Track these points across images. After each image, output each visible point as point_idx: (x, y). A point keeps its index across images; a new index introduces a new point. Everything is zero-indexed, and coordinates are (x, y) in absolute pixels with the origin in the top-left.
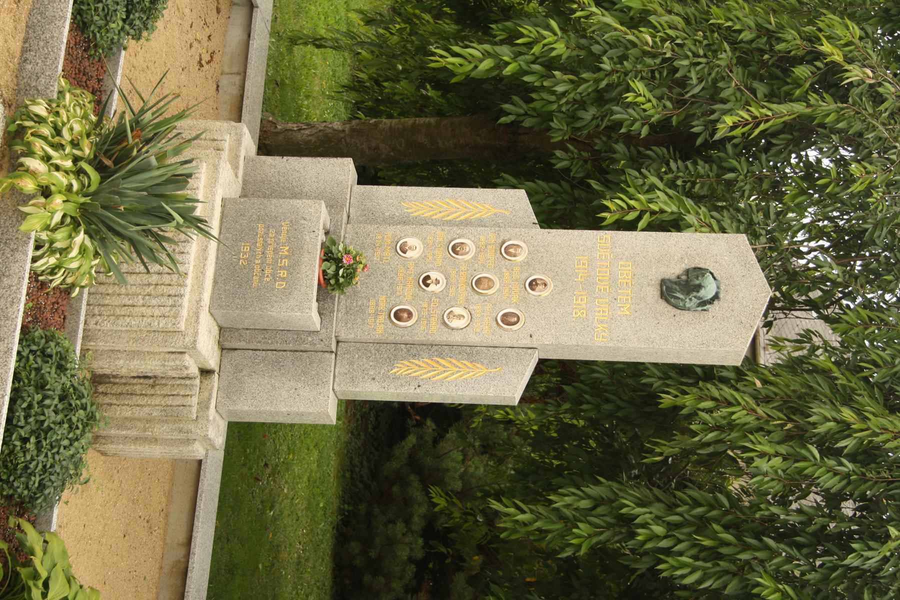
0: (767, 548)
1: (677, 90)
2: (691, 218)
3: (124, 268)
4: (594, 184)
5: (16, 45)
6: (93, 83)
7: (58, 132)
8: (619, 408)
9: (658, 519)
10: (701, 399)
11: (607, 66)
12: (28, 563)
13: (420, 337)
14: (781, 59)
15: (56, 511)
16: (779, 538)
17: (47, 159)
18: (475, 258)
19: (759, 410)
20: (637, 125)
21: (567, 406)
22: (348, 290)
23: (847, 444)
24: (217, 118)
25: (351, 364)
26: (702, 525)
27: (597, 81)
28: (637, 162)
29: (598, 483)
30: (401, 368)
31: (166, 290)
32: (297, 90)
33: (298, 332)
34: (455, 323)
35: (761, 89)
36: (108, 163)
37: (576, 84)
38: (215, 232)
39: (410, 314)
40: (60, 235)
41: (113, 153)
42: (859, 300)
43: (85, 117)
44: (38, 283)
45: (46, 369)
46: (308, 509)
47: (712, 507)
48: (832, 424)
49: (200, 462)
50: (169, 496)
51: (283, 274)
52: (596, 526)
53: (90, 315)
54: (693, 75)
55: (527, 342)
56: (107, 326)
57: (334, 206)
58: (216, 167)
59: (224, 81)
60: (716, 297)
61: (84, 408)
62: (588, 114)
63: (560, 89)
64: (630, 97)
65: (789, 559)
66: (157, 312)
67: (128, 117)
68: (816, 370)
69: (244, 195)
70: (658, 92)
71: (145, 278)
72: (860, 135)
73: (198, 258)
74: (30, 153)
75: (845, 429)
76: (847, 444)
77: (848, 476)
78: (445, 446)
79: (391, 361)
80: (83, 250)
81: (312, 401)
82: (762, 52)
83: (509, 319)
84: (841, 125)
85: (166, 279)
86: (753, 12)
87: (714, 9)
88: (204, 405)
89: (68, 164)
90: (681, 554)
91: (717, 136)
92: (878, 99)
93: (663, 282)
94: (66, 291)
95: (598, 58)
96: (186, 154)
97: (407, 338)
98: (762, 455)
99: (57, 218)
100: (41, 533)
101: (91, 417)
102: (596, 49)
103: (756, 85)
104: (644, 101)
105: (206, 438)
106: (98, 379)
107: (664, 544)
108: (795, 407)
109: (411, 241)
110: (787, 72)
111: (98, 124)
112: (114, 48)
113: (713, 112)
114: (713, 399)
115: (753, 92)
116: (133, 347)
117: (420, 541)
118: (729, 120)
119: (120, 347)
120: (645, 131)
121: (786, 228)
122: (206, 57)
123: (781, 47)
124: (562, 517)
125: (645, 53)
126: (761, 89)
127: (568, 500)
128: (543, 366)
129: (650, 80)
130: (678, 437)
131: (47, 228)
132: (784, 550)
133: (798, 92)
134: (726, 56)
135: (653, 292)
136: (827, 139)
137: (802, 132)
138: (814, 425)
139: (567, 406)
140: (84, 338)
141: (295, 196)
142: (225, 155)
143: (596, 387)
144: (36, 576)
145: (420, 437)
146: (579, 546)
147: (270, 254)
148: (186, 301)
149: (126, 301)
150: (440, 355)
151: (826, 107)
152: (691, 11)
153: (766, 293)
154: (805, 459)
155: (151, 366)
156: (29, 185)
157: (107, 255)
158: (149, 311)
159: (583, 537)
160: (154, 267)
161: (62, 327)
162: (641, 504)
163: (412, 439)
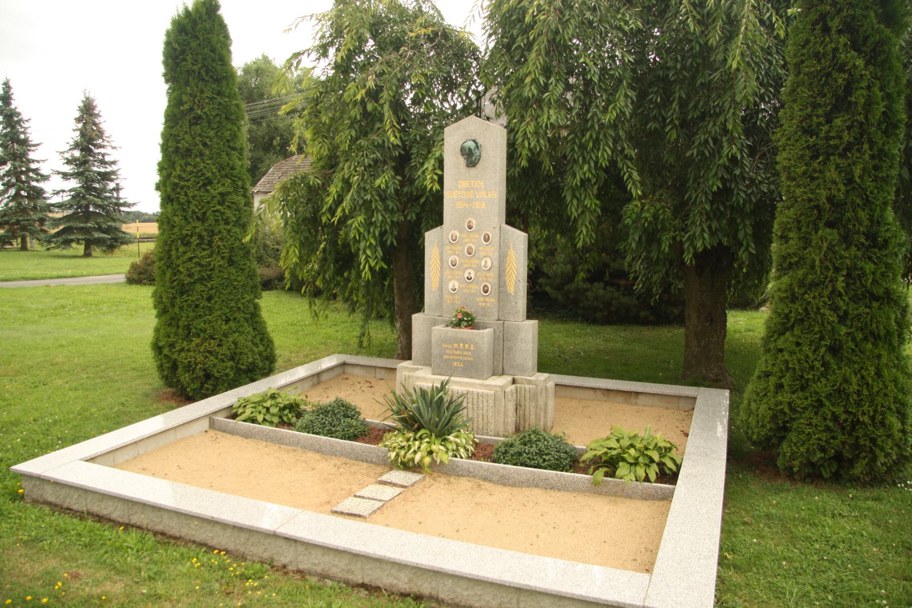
0: (592, 117)
1: (379, 164)
2: (437, 154)
3: (465, 419)
4: (422, 200)
5: (365, 465)
6: (380, 433)
7: (403, 447)
8: (530, 187)
9: (581, 168)
10: (524, 147)
11: (368, 197)
12: (600, 457)
13: (496, 280)
14: (364, 117)
15: (577, 447)
16: (587, 111)
17: (415, 452)
18: (458, 255)
19: (528, 120)
20: (396, 182)
21: (531, 212)
22: (474, 315)
23: (542, 80)
24: (395, 379)
25: (509, 313)
26: (583, 147)
27: (376, 201)
28: (412, 181)
29: (565, 197)
30: (511, 290)
31: (475, 400)
32: (383, 345)
33: (495, 339)
34: (489, 264)
35: (378, 125)
36: (416, 426)
37: (378, 211)
38: (447, 378)
39: (485, 286)
40: (450, 447)
41: (412, 423)
42: (475, 78)
43: (396, 436)
44: (473, 456)
45: (512, 452)
46: (580, 337)
47: (575, 142)
48: (533, 87)
49: (556, 385)
50: (572, 398)
51: (467, 346)
52: (586, 196)
53: (487, 434)
54: (372, 156)
55: (497, 230)
56: (492, 427)
57: (434, 323)
58: (418, 378)
59: (379, 376)
60: (474, 141)
61: (530, 435)
62: (391, 205)
63: (380, 218)
64: (383, 186)
65: (597, 107)
66: (486, 404)
67: (395, 417)
68: (508, 96)
69: (430, 365)
70: (381, 173)
71: (470, 409)
72: (398, 80)
73: (459, 385)
74: (413, 460)
75: (535, 81)
76: (542, 80)
77: (557, 81)
78: (550, 273)
79: (507, 294)
80: (457, 437)
81: (527, 332)
82: (361, 125)
83: (487, 239)
84: (394, 88)
85: (470, 400)
86: (342, 131)
87: (342, 149)
88: (529, 382)
89: (417, 443)
90: (597, 157)
91: (400, 144)
92: (383, 73)
93: (468, 166)
94: (476, 445)
95: (365, 201)
96: (412, 391)
97: (497, 287)
98: (549, 119)
99: (442, 448)
100: (586, 452)
101: (534, 432)
102: (361, 202)
103: (376, 128)
104: (385, 180)
105: (545, 381)
106: (517, 430)
107: (592, 164)
108: (526, 104)
109: (450, 286)
110: (370, 114)
111: (399, 430)
112: (364, 423)
113: (389, 148)
114: (523, 141)
115: (379, 129)
116: (502, 415)
117: (596, 284)
118: (392, 139)
119: (502, 420)
120: (399, 178)
121: (442, 112)
122: (368, 384)
123: (358, 117)
124: (583, 212)
125: (362, 179)
126: (378, 125)
127: (573, 210)
128: (509, 222)
129: (375, 176)
130: (541, 158)
131: (447, 452)
132: (593, 110)
133: (379, 108)
134: (363, 142)
135: (473, 171)
136: (401, 95)
137: (397, 106)
138: (533, 95)
139: (531, 212)
140: (498, 436)
141: (430, 342)
142: (411, 374)
143: (522, 198)
144: (606, 453)
145: (547, 285)
146: (596, 204)
147: (458, 352)
148: (480, 391)
149: (481, 418)
150: (504, 271)
151: (385, 95)
152: (342, 159)
153: (473, 117)
154: (549, 100)
155: (511, 407)
156: (427, 460)
157: (459, 426)
158: (485, 407)
159: (591, 202)
160: (464, 404)
161: (493, 446)
162: (574, 175)
163: (548, 289)
